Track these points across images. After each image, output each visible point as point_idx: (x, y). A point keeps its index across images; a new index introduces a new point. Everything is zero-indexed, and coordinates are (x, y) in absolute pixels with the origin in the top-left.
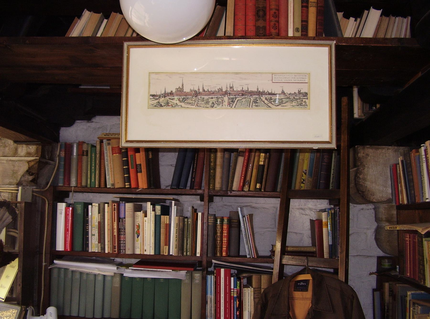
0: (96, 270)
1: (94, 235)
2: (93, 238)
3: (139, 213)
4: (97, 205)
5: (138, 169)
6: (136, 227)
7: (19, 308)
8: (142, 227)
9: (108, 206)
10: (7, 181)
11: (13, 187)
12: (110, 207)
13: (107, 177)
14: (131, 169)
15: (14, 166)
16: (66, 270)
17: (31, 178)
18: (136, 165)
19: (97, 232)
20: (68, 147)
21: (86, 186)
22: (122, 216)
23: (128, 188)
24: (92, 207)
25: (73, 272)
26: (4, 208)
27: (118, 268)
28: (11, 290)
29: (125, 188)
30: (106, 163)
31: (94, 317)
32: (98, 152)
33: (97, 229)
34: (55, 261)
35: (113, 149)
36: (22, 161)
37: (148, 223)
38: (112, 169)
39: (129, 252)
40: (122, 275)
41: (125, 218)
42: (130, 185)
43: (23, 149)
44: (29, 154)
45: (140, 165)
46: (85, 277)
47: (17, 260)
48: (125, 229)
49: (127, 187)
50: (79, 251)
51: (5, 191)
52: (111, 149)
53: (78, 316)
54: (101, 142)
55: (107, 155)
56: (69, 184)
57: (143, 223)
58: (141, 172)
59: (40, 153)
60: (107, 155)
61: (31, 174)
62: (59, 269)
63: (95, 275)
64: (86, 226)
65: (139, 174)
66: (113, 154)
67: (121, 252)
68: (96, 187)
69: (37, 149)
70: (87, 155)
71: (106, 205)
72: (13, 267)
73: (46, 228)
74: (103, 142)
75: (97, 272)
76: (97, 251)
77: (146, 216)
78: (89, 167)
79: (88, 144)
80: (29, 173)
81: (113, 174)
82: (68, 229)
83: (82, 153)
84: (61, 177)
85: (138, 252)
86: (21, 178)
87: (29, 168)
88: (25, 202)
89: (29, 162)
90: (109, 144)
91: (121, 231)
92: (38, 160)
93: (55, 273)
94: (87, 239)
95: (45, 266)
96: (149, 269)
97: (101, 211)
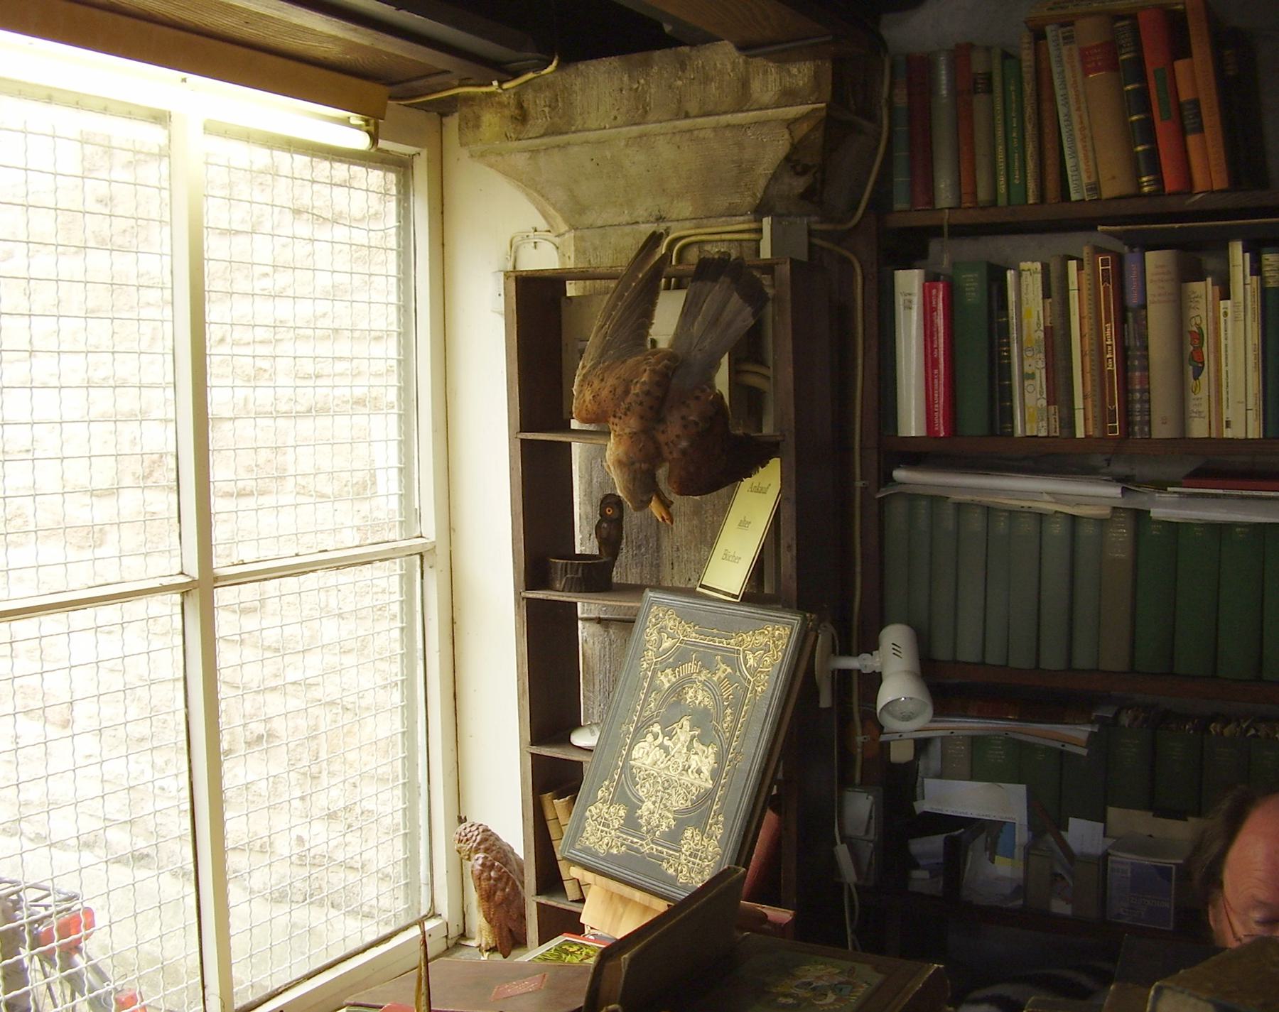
0: (1047, 497)
1: (1032, 376)
2: (1030, 389)
3: (1197, 288)
4: (1038, 265)
5: (1186, 120)
6: (1188, 338)
7: (796, 620)
8: (1211, 335)
9: (1080, 268)
10: (721, 202)
11: (742, 223)
12: (1087, 268)
13: (1069, 163)
14: (1158, 123)
15: (740, 145)
16: (936, 500)
17: (800, 184)
18: (1179, 107)
19: (1042, 364)
20: (919, 70)
21: (994, 203)
22: (1133, 299)
23: (1149, 194)
24: (1019, 275)
25: (959, 506)
26: (725, 280)
27: (1124, 490)
28: (757, 572)
29: (1139, 195)
30: (1062, 111)
31: (1037, 667)
32: (1028, 75)
33: (1042, 356)
34: (900, 474)
35: (1084, 55)
36: (764, 123)
37: (1236, 319)
38: (1087, 132)
39: (1162, 430)
40: (1140, 516)
41: (1144, 307)
42: (1159, 181)
43: (767, 81)
44: (789, 96)
45: (1196, 103)
46: (1002, 525)
47: (775, 465)
48: (1146, 348)
49: (1146, 189)
50: (977, 431)
51: (717, 237)
52: (1077, 58)
53: (983, 663)
54: (1039, 36)
55: (1064, 83)
56: (931, 201)
57: (1217, 323)
58: (1200, 129)
59: (827, 88)
60: (1064, 83)
61: (799, 168)
62: (912, 498)
63: (1041, 517)
64: (1001, 345)
65: (1192, 140)
66: (1086, 73)
67: (1134, 433)
68: (1031, 201)
69: (816, 76)
70: (989, 90)
71: (1073, 265)
72: (760, 490)
73: (860, 361)
74: (1045, 38)
75: (1049, 507)
76: (1043, 433)
77: (1226, 295)
78: (1000, 132)
79: (988, 49)
80: (793, 167)
81: (1090, 148)
82: (937, 360)
83: (972, 85)
84: (900, 179)
85: (1198, 429)
86: (767, 187)
87: (795, 148)
88: (792, 261)
89: (790, 124)
90: (1068, 39)
91: (1131, 353)
92: (824, 113)
93: (897, 513)
94: (1007, 393)
95: (864, 489)
96: (1245, 493)
97: (1054, 288)
